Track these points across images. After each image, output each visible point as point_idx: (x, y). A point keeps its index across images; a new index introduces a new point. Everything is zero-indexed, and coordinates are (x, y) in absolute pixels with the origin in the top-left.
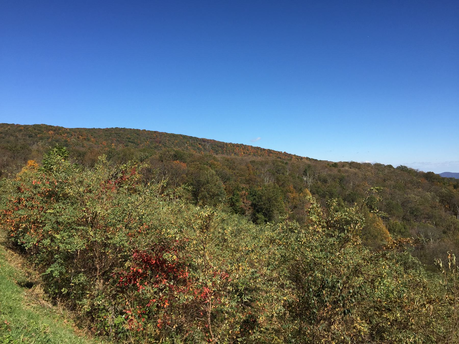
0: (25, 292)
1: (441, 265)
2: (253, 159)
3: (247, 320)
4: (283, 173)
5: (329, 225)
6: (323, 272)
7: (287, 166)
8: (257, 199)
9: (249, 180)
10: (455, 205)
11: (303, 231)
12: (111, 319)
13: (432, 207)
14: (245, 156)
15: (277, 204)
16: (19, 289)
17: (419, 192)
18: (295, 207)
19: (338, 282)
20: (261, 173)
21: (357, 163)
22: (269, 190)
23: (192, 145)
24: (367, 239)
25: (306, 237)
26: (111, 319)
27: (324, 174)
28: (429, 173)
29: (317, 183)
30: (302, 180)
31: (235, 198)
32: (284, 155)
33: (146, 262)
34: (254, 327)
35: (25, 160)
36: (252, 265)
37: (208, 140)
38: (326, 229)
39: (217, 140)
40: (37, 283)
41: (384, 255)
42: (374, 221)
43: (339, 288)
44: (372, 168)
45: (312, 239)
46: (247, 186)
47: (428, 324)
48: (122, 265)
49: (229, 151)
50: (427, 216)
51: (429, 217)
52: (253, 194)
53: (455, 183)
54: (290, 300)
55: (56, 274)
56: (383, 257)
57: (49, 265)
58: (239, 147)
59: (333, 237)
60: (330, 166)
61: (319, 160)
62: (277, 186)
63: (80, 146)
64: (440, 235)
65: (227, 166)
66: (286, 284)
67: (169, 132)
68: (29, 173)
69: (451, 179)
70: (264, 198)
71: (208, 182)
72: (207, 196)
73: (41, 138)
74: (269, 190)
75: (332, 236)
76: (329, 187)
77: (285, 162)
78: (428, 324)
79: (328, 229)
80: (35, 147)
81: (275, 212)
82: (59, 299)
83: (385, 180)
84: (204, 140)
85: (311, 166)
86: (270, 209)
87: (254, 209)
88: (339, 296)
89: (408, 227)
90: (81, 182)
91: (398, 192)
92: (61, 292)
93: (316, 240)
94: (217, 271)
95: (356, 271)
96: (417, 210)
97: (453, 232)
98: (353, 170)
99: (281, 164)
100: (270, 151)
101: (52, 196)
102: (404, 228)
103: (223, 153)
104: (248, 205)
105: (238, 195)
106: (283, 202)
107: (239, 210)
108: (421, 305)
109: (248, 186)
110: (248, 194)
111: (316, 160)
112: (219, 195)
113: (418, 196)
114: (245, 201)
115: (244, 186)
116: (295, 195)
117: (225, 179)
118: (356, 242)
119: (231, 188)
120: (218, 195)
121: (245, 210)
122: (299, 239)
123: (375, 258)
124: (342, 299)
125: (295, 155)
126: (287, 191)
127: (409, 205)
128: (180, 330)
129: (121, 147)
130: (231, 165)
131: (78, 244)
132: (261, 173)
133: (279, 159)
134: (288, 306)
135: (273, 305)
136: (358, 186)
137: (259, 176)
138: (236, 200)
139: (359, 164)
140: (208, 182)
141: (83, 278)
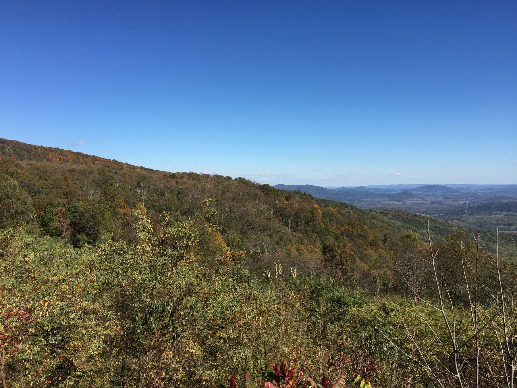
1: (269, 275)
2: (73, 168)
3: (61, 365)
4: (112, 185)
5: (162, 242)
6: (152, 297)
7: (116, 177)
8: (78, 217)
9: (67, 193)
10: (287, 216)
11: (130, 252)
13: (267, 219)
14: (61, 163)
15: (104, 222)
17: (256, 204)
18: (127, 225)
19: (168, 305)
20: (84, 185)
21: (196, 174)
22: (94, 205)
24: (205, 256)
25: (133, 258)
27: (161, 185)
28: (265, 185)
29: (152, 196)
30: (135, 193)
31: (48, 216)
32: (113, 163)
34: (70, 372)
37: (8, 141)
38: (156, 248)
39: (22, 142)
41: (217, 271)
42: (213, 236)
43: (169, 312)
44: (211, 179)
45: (141, 260)
46: (65, 201)
47: (259, 337)
49: (39, 156)
50: (263, 229)
51: (265, 229)
52: (72, 210)
53: (287, 195)
56: (216, 273)
58: (53, 151)
59: (164, 256)
60: (168, 177)
61: (155, 169)
62: (104, 200)
64: (274, 246)
65: (35, 175)
66: (107, 316)
69: (284, 191)
70: (87, 215)
71: (7, 197)
72: (7, 214)
74: (94, 205)
75: (163, 255)
76: (166, 200)
77: (114, 171)
78: (259, 337)
79: (159, 246)
81: (102, 231)
83: (224, 193)
85: (143, 177)
86: (94, 228)
87: (74, 229)
88: (169, 321)
89: (245, 240)
91: (236, 205)
93: (145, 262)
94: (12, 311)
95: (189, 291)
96: (254, 222)
97: (285, 243)
99: (111, 176)
100: (95, 159)
102: (242, 241)
103: (30, 159)
104: (65, 224)
105: (51, 212)
106: (111, 220)
107: (54, 231)
108: (253, 318)
109: (66, 200)
110: (66, 210)
111: (152, 170)
112: (24, 213)
113: (255, 208)
114: (62, 219)
115: (60, 200)
116: (127, 210)
117: (33, 192)
118: (189, 259)
119: (42, 204)
120: (23, 213)
121: (62, 231)
122: (124, 261)
123: (208, 275)
124: (172, 324)
125: (127, 164)
126: (117, 206)
127: (247, 218)
130: (43, 175)
132: (84, 185)
133: (107, 168)
134: (109, 341)
135: (91, 343)
136: (197, 199)
137: (81, 189)
138: (49, 219)
139: (199, 175)
140: (7, 197)
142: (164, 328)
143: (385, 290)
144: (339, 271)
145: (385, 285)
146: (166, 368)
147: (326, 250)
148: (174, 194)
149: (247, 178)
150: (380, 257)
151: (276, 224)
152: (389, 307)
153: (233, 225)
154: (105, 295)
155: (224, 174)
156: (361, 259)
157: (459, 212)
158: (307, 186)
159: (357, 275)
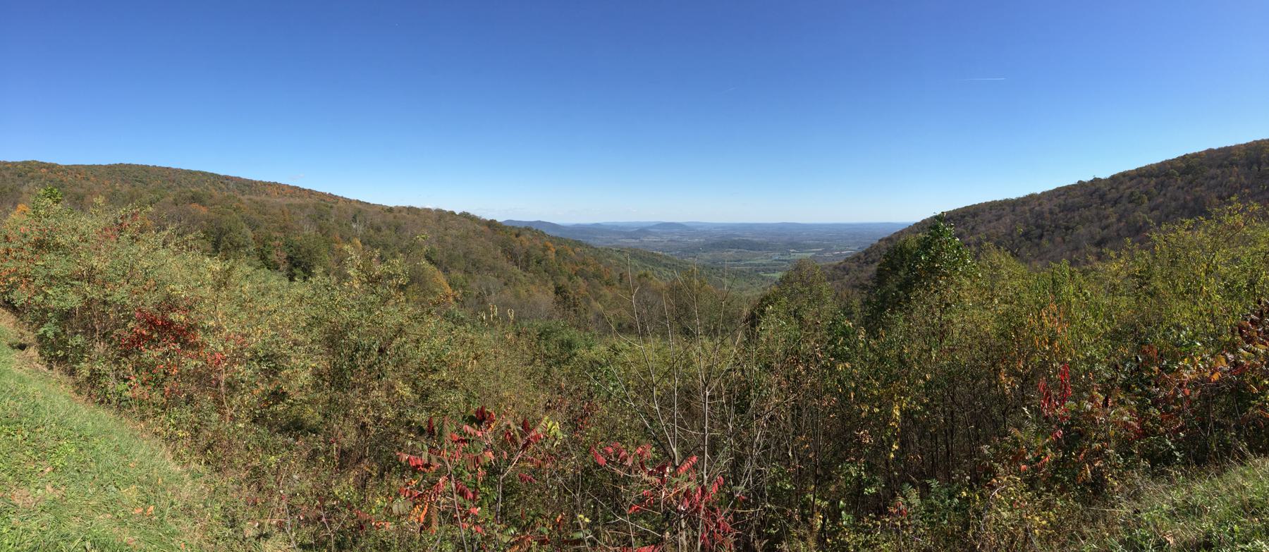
0: (18, 353)
12: (112, 385)
16: (10, 350)
23: (213, 184)
26: (112, 385)
27: (378, 220)
28: (492, 221)
30: (350, 228)
31: (267, 249)
33: (151, 323)
35: (15, 205)
36: (273, 327)
40: (30, 345)
41: (429, 312)
46: (282, 235)
48: (125, 325)
51: (492, 269)
52: (289, 245)
54: (320, 367)
55: (50, 334)
57: (42, 325)
62: (319, 235)
63: (71, 186)
67: (185, 167)
68: (19, 220)
73: (33, 178)
80: (25, 189)
82: (54, 364)
84: (227, 178)
85: (359, 210)
90: (75, 230)
92: (58, 355)
96: (479, 261)
98: (410, 217)
99: (324, 209)
100: (311, 192)
101: (40, 245)
103: (251, 193)
117: (254, 226)
128: (190, 399)
129: (126, 188)
130: (262, 208)
131: (73, 301)
134: (318, 374)
141: (79, 339)
142: (370, 366)
143: (620, 329)
144: (572, 313)
145: (620, 325)
146: (375, 405)
147: (559, 290)
148: (389, 229)
149: (472, 213)
150: (616, 297)
151: (504, 263)
152: (618, 347)
153: (455, 264)
154: (315, 330)
155: (447, 208)
156: (596, 299)
157: (693, 250)
158: (539, 222)
159: (591, 317)
